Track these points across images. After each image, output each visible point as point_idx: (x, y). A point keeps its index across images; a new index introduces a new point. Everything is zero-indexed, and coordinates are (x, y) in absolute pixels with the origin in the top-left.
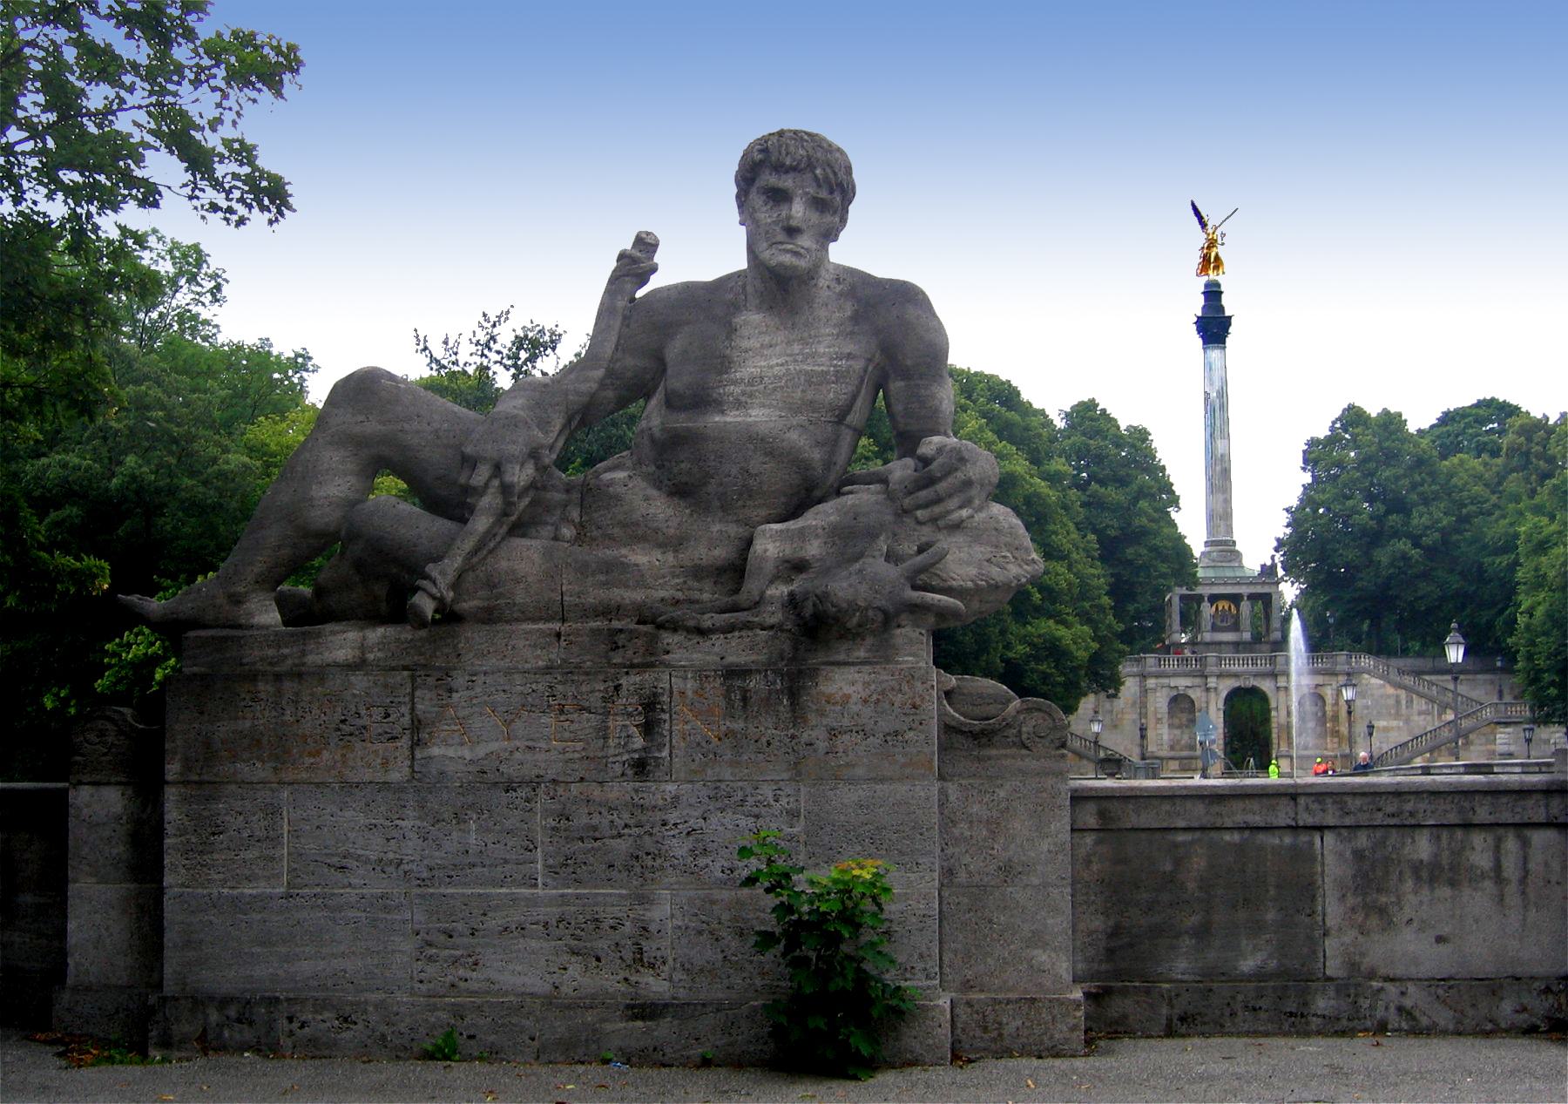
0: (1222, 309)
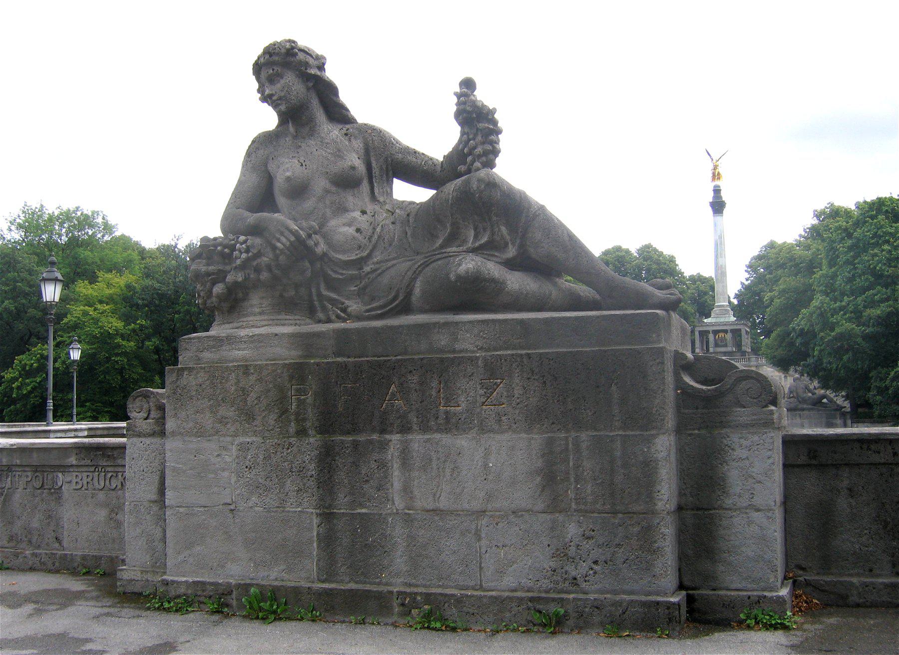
0: (721, 197)
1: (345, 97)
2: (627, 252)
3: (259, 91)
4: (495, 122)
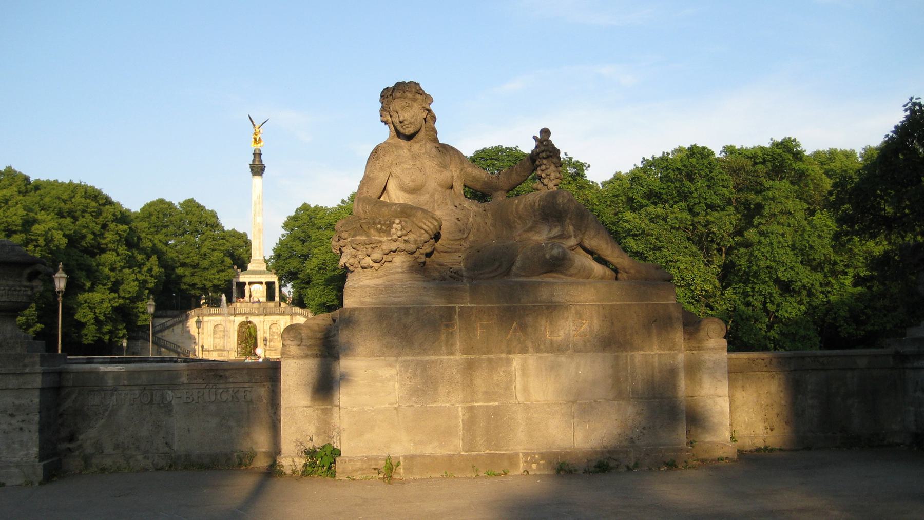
2: (170, 205)
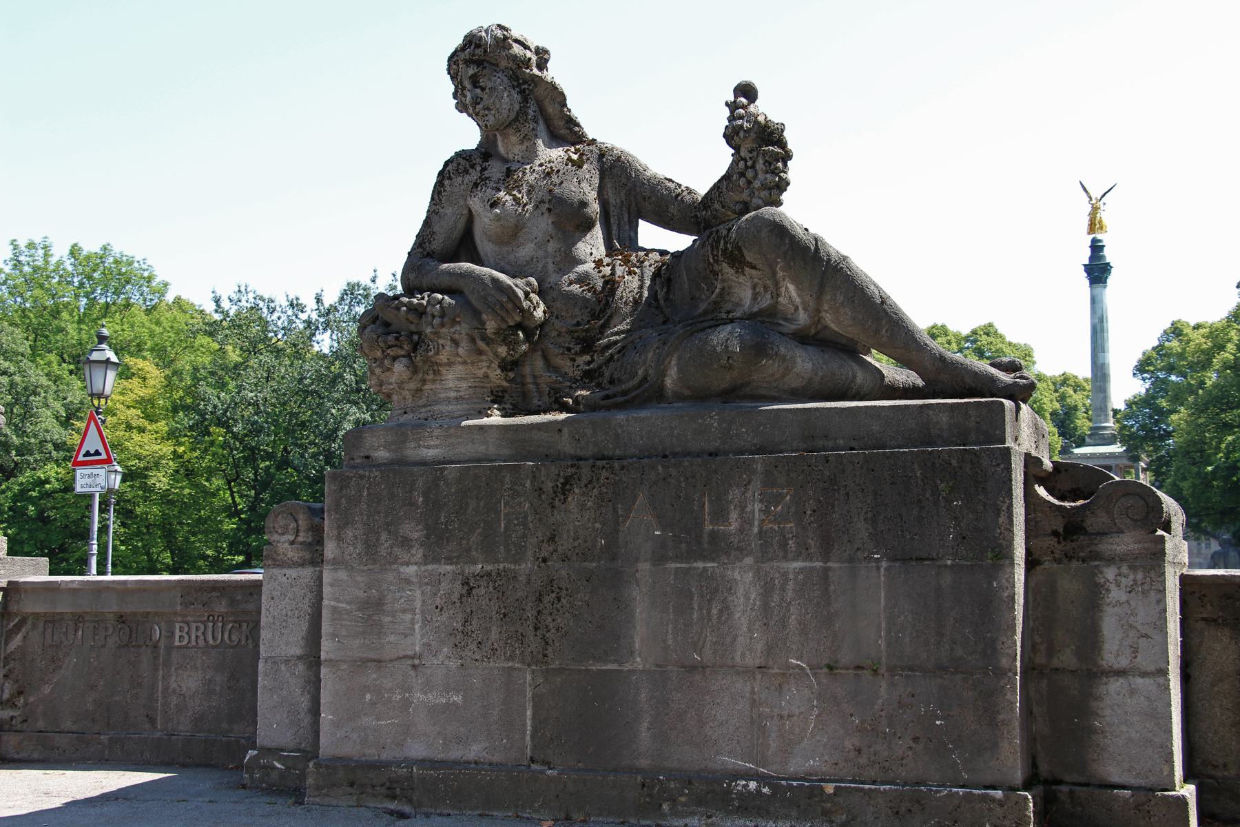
1: (577, 107)
3: (455, 96)
4: (782, 143)
